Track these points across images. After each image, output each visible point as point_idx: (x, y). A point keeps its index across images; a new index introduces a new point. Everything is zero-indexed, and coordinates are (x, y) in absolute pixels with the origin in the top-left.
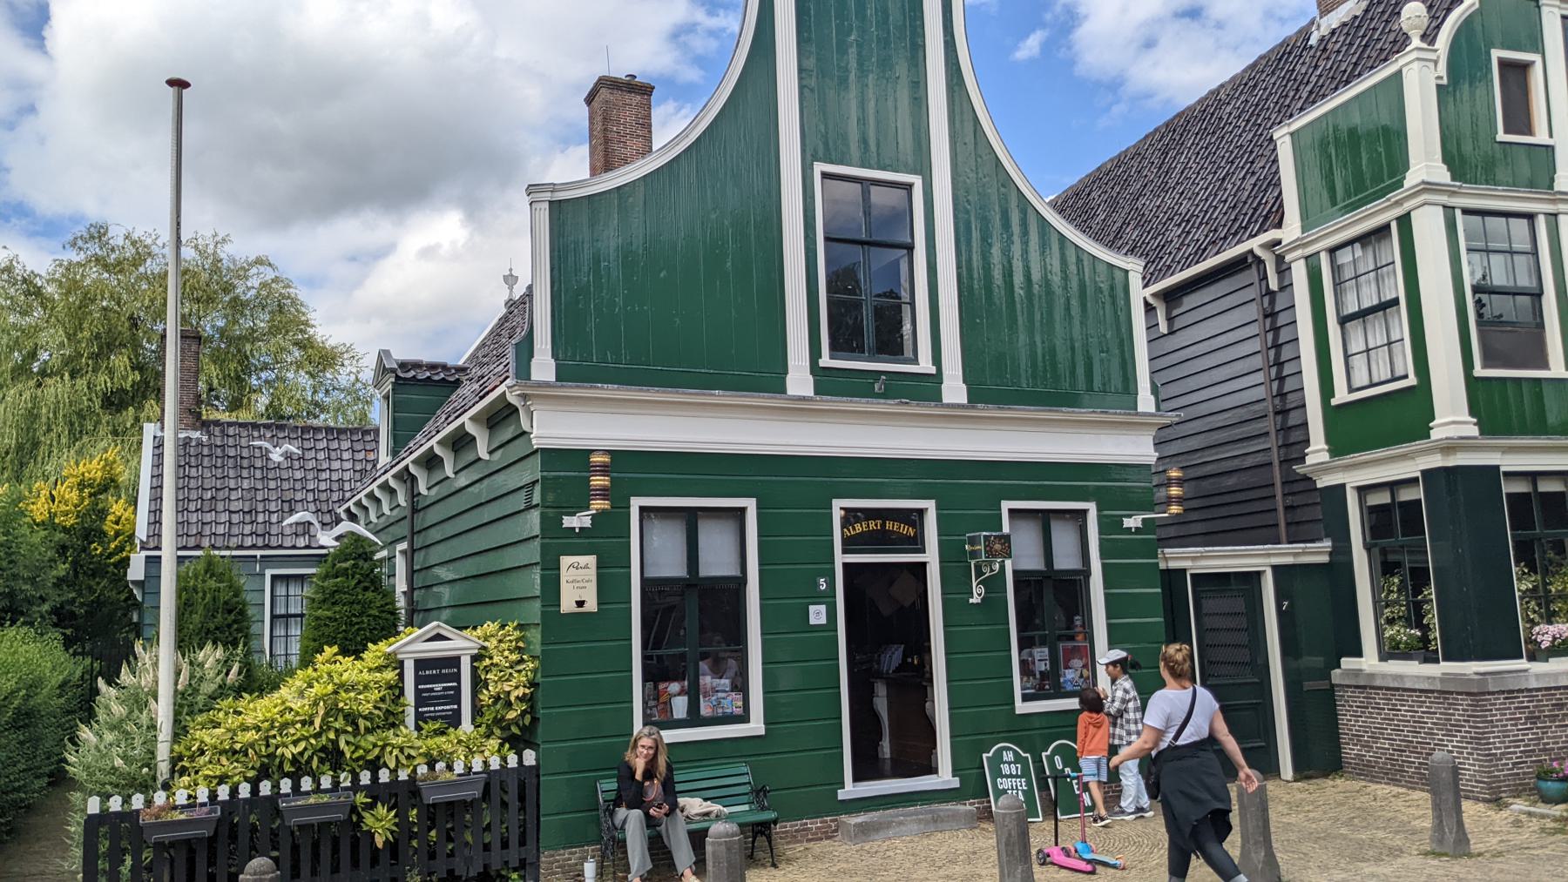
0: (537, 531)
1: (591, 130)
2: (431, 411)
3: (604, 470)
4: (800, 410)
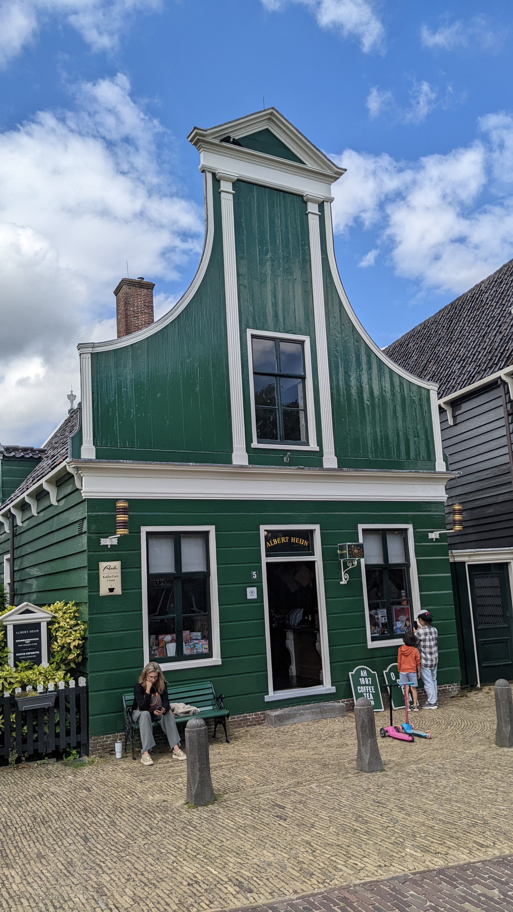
0: (85, 548)
1: (118, 310)
2: (24, 475)
3: (125, 511)
4: (240, 473)
